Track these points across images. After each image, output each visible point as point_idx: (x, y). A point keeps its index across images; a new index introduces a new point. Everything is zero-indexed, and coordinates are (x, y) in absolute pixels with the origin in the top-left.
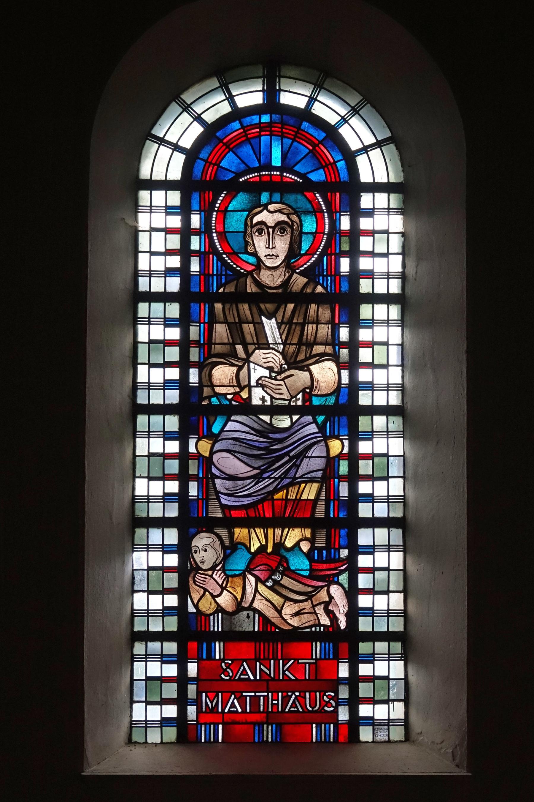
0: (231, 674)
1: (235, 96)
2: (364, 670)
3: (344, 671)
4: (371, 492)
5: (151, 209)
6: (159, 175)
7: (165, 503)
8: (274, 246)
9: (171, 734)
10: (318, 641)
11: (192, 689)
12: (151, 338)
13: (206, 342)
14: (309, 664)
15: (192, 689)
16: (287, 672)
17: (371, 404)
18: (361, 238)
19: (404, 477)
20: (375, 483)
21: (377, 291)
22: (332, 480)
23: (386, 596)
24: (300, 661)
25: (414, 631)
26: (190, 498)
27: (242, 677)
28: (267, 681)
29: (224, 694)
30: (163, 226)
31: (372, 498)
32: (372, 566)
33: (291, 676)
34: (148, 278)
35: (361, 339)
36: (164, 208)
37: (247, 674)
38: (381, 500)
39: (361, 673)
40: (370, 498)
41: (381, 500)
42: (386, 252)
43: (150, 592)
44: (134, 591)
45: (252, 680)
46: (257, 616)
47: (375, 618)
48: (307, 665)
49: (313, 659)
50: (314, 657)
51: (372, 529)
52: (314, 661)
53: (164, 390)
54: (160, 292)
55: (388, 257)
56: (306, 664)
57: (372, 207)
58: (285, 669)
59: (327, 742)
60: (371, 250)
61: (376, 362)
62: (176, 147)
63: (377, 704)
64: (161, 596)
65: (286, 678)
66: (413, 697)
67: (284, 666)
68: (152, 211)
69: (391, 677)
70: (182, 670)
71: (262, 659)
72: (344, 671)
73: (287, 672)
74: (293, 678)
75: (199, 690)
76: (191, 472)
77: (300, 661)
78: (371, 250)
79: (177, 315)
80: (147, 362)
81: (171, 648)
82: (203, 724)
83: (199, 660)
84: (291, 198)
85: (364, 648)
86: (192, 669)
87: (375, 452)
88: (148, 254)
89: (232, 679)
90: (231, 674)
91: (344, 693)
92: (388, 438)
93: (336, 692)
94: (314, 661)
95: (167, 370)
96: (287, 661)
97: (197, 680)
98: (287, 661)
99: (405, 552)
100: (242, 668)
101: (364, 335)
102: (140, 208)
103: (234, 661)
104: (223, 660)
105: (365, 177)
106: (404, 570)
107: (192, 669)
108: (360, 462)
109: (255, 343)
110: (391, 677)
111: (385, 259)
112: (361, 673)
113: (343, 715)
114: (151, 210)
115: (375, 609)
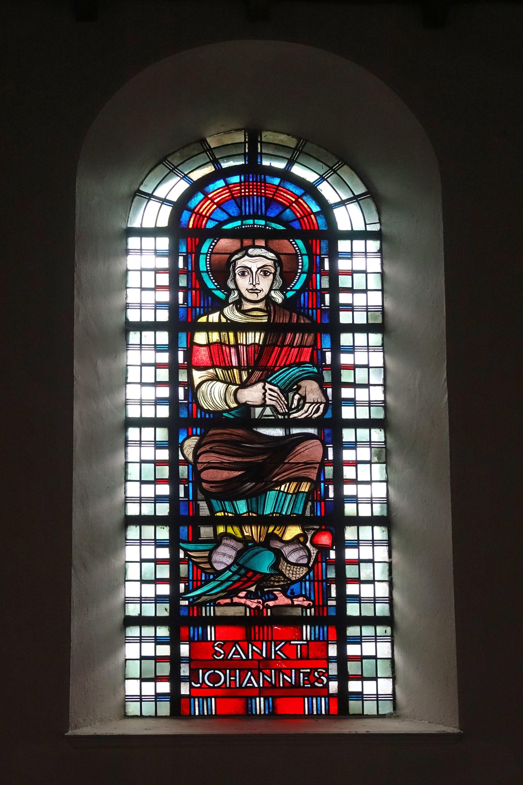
0: (222, 652)
1: (141, 225)
2: (352, 650)
3: (333, 651)
4: (353, 397)
5: (140, 443)
6: (149, 224)
7: (157, 604)
8: (258, 282)
9: (165, 708)
10: (308, 625)
11: (185, 670)
12: (142, 655)
13: (193, 270)
14: (300, 644)
15: (185, 670)
16: (278, 652)
17: (351, 322)
18: (344, 467)
19: (387, 481)
20: (362, 585)
21: (361, 514)
22: (320, 564)
23: (365, 295)
24: (292, 642)
25: (393, 419)
26: (180, 401)
27: (234, 656)
28: (259, 660)
29: (217, 699)
30: (153, 362)
31: (361, 696)
32: (360, 654)
33: (282, 655)
34: (139, 703)
35: (347, 593)
36: (154, 305)
37: (239, 654)
38: (362, 404)
39: (343, 396)
40: (350, 308)
41: (362, 404)
42: (369, 480)
43: (142, 680)
44: (126, 481)
45: (244, 660)
46: (248, 610)
47: (362, 604)
48: (299, 646)
49: (304, 641)
50: (304, 638)
51: (354, 430)
52: (305, 642)
53: (155, 503)
54: (150, 516)
55: (371, 485)
56: (297, 645)
57: (359, 635)
58: (277, 649)
59: (319, 715)
60: (355, 478)
61: (359, 479)
62: (164, 201)
63: (355, 293)
64: (153, 486)
65: (278, 658)
66: (399, 675)
67: (275, 647)
68: (142, 349)
69: (378, 657)
70: (175, 650)
71: (253, 641)
72: (333, 651)
73: (278, 652)
74: (284, 657)
75: (191, 667)
76: (182, 693)
77: (292, 642)
78: (355, 478)
79: (166, 342)
80: (139, 479)
81: (163, 632)
82: (197, 697)
83: (191, 641)
84: (275, 244)
85: (352, 631)
86: (185, 650)
87: (363, 654)
88: (139, 483)
89: (225, 659)
90: (222, 652)
91: (333, 668)
92: (377, 694)
93: (327, 670)
94: (305, 642)
95: (158, 486)
96: (280, 642)
97: (190, 660)
98: (280, 642)
99: (392, 643)
100: (234, 648)
101: (350, 554)
102: (129, 442)
103: (226, 643)
104: (216, 641)
105: (343, 225)
106: (384, 367)
107: (185, 650)
108: (347, 567)
109: (244, 344)
110: (378, 657)
111: (369, 486)
112: (343, 396)
113: (333, 686)
114: (141, 347)
115: (364, 693)
